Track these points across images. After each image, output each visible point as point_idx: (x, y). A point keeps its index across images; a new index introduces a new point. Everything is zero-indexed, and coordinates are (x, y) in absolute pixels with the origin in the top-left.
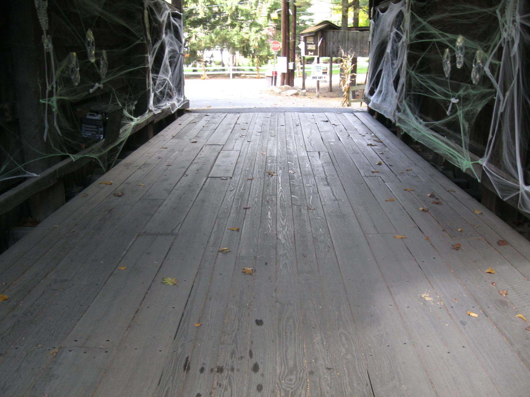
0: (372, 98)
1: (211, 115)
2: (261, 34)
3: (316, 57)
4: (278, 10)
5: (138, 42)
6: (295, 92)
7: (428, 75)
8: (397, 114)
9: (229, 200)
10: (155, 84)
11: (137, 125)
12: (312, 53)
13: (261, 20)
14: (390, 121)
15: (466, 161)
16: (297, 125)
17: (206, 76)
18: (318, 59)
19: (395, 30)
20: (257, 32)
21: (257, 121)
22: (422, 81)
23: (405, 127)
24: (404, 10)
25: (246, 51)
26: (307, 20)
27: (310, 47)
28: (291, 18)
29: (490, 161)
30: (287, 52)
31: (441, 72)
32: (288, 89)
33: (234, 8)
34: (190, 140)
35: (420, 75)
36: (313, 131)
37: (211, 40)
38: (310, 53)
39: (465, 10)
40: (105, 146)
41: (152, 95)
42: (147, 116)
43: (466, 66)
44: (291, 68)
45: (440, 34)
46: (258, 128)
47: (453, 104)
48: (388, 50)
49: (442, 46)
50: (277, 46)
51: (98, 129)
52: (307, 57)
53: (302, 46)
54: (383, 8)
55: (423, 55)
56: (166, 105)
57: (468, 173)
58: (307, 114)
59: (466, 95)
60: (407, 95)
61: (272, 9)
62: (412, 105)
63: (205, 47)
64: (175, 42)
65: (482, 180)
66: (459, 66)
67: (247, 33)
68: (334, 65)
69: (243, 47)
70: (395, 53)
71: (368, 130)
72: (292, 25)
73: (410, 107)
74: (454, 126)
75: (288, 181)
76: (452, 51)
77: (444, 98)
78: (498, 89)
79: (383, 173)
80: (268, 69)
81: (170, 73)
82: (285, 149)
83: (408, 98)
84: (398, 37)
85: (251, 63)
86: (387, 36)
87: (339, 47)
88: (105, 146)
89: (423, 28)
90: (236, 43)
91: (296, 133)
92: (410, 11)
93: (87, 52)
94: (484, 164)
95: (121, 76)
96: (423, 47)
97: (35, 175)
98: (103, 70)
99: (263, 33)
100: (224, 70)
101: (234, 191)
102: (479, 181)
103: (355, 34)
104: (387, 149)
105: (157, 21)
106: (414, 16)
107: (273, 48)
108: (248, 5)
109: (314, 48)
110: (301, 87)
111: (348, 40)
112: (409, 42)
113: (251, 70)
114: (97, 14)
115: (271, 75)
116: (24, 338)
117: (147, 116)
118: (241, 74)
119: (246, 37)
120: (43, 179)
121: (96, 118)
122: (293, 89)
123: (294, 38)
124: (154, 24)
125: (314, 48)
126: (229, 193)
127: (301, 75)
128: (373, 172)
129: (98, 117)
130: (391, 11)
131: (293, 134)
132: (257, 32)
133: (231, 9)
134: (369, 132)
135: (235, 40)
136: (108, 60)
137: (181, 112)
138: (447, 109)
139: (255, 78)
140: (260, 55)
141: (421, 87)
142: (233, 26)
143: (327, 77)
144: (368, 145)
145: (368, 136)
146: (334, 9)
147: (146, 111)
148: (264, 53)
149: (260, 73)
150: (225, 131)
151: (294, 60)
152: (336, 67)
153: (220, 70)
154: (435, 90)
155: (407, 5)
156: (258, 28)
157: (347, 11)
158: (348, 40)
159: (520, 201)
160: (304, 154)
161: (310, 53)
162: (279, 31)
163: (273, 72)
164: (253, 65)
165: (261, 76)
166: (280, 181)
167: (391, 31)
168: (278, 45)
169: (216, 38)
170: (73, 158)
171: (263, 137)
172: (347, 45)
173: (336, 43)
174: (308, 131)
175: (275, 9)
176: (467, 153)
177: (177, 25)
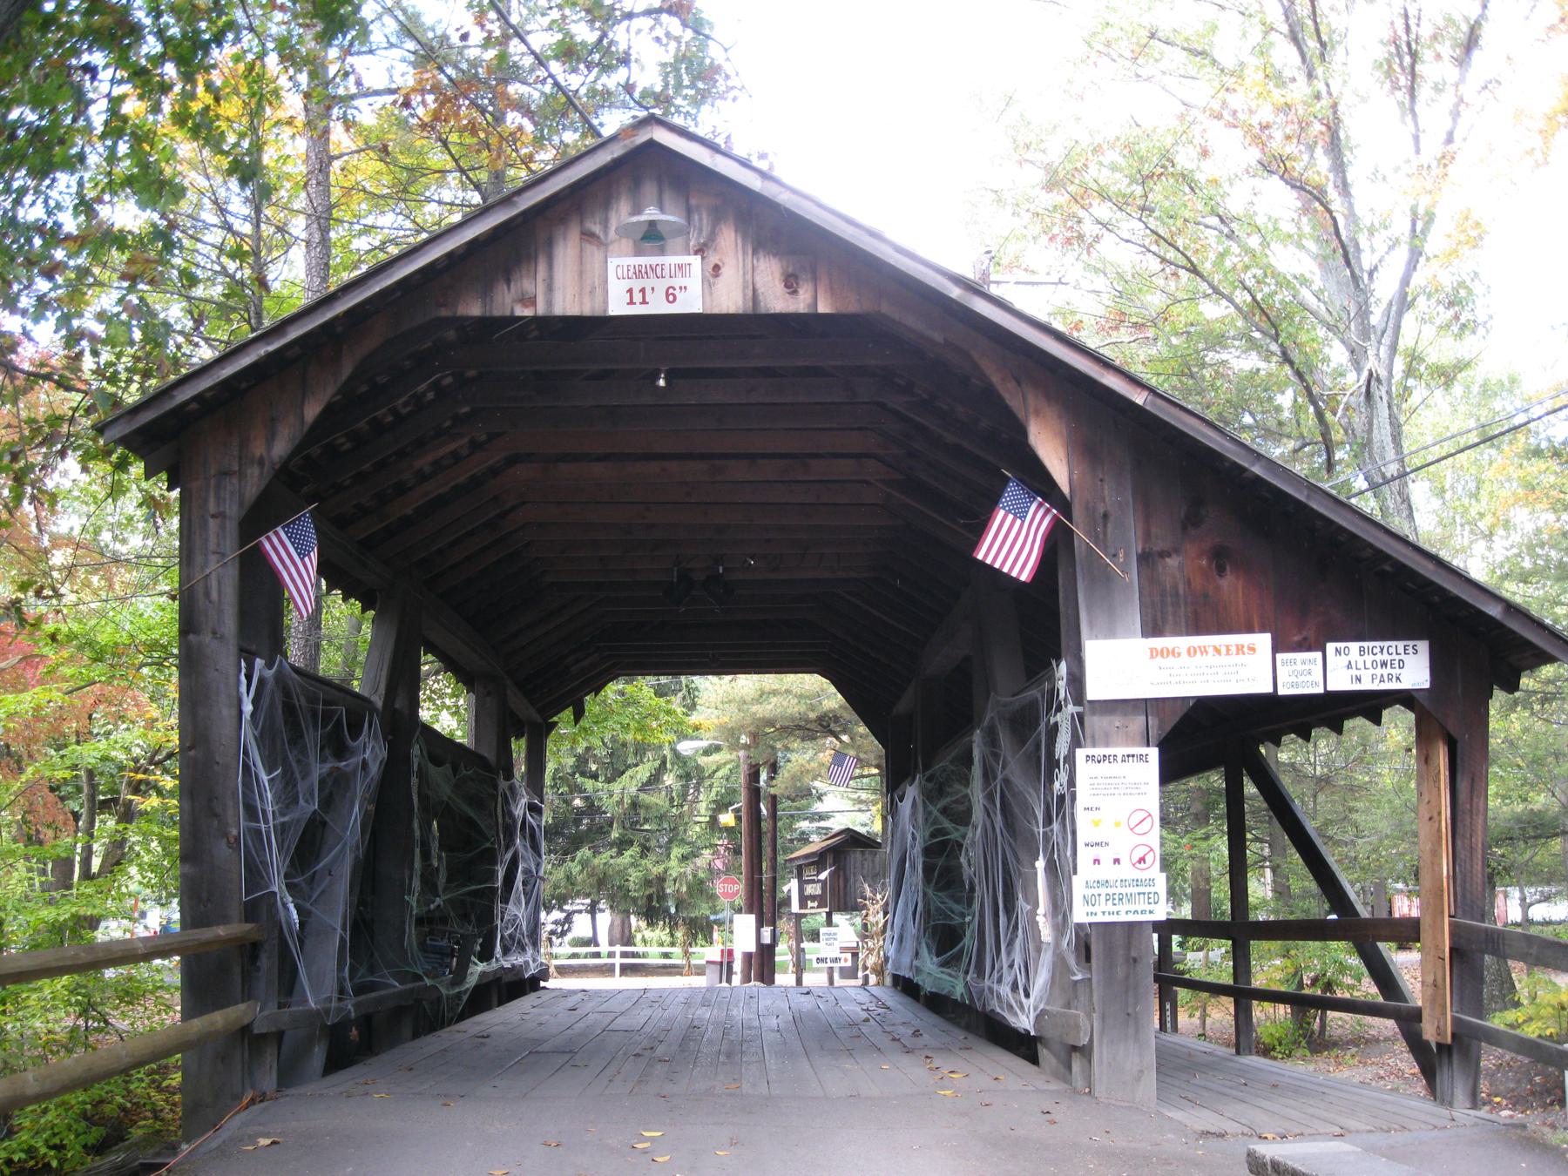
4: (736, 806)
5: (488, 845)
12: (816, 904)
20: (684, 858)
28: (765, 826)
30: (756, 903)
33: (627, 801)
38: (810, 904)
53: (791, 887)
56: (516, 959)
61: (721, 805)
64: (530, 854)
69: (650, 898)
98: (442, 879)
99: (700, 862)
109: (819, 892)
114: (446, 799)
115: (719, 959)
125: (819, 892)
133: (621, 802)
134: (875, 1000)
140: (693, 915)
142: (622, 845)
161: (810, 904)
168: (736, 887)
169: (582, 871)
170: (428, 982)
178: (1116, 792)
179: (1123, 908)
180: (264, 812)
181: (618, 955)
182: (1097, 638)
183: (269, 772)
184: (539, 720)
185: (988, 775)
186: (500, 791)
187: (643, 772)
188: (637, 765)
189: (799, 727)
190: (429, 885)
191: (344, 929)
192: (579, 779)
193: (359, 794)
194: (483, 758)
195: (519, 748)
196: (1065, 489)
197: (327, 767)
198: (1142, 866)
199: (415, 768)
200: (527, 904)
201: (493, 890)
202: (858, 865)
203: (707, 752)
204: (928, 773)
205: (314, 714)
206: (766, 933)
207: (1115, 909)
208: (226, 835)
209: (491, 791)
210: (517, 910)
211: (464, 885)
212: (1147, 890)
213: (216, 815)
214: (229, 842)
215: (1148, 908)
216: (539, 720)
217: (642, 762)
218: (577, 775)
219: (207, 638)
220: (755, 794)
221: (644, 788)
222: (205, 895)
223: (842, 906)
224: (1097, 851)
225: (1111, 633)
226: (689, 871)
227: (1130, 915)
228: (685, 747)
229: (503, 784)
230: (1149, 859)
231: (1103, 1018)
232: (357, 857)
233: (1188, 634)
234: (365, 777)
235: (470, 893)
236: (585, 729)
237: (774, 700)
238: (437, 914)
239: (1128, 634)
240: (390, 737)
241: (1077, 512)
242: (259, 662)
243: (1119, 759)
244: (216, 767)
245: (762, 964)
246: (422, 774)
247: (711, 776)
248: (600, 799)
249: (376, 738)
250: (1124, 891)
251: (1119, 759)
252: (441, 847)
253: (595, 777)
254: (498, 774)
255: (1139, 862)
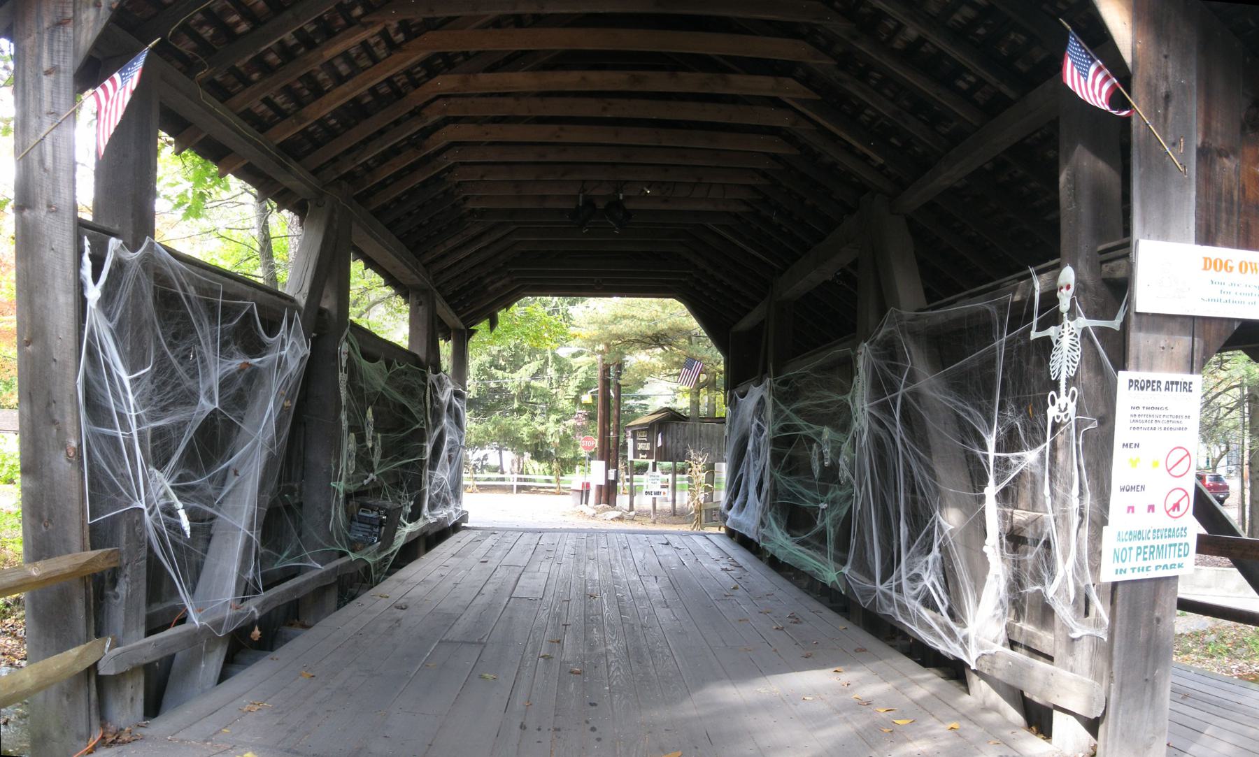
0: (729, 513)
1: (501, 533)
2: (564, 425)
3: (650, 462)
4: (593, 390)
5: (418, 426)
6: (617, 514)
7: (797, 478)
8: (761, 530)
9: (543, 617)
10: (430, 483)
11: (411, 534)
12: (645, 456)
13: (564, 404)
14: (752, 540)
15: (831, 573)
16: (625, 548)
17: (475, 487)
18: (654, 465)
19: (756, 421)
20: (558, 421)
21: (568, 542)
22: (789, 485)
23: (770, 546)
24: (766, 395)
25: (539, 451)
26: (637, 407)
27: (641, 446)
28: (613, 404)
29: (854, 567)
31: (810, 471)
32: (608, 510)
33: (523, 385)
34: (478, 559)
35: (787, 478)
36: (647, 555)
37: (487, 432)
39: (826, 397)
40: (380, 551)
41: (427, 497)
42: (421, 523)
43: (834, 464)
44: (612, 477)
45: (806, 425)
46: (569, 549)
47: (823, 510)
48: (750, 448)
49: (810, 441)
50: (590, 443)
51: (372, 529)
52: (638, 462)
54: (742, 391)
55: (789, 452)
56: (442, 513)
57: (834, 586)
58: (638, 536)
59: (834, 498)
60: (772, 505)
61: (583, 389)
62: (779, 516)
63: (476, 444)
64: (454, 429)
65: (846, 591)
66: (826, 463)
67: (542, 424)
68: (678, 476)
70: (757, 451)
71: (722, 553)
72: (614, 413)
73: (776, 519)
74: (822, 536)
75: (616, 603)
76: (820, 446)
77: (813, 505)
78: (855, 485)
79: (739, 597)
80: (575, 479)
81: (449, 470)
82: (610, 573)
83: (773, 509)
84: (760, 430)
85: (547, 471)
86: (747, 430)
87: (687, 447)
88: (380, 551)
89: (787, 418)
90: (526, 438)
91: (625, 556)
92: (771, 397)
93: (365, 433)
94: (846, 572)
95: (394, 468)
96: (789, 441)
97: (319, 566)
98: (376, 459)
100: (503, 479)
101: (548, 611)
102: (843, 592)
103: (710, 428)
104: (747, 574)
105: (438, 400)
106: (962, 417)
107: (583, 447)
108: (546, 381)
109: (648, 448)
110: (628, 508)
111: (700, 436)
112: (771, 436)
113: (548, 481)
114: (380, 389)
115: (581, 489)
116: (981, 31)
117: (421, 523)
118: (531, 487)
119: (541, 428)
120: (327, 572)
121: (371, 515)
122: (615, 510)
123: (618, 432)
124: (436, 406)
125: (648, 448)
126: (541, 612)
127: (627, 491)
128: (726, 596)
129: (374, 515)
130: (752, 396)
131: (619, 558)
132: (558, 421)
134: (725, 556)
135: (525, 433)
136: (382, 446)
137: (456, 528)
138: (817, 518)
139: (554, 493)
141: (790, 494)
142: (520, 411)
143: (669, 492)
144: (723, 569)
145: (724, 561)
146: (679, 391)
147: (419, 518)
148: (568, 455)
149: (561, 485)
150: (524, 552)
151: (616, 466)
152: (682, 479)
153: (498, 479)
154: (803, 496)
155: (768, 389)
156: (559, 416)
157: (698, 394)
158: (700, 436)
159: (877, 604)
160: (635, 578)
162: (593, 423)
163: (583, 484)
164: (551, 474)
165: (563, 491)
166: (606, 603)
167: (752, 423)
169: (494, 429)
170: (353, 556)
171: (579, 560)
172: (698, 443)
173: (681, 441)
174: (641, 555)
175: (588, 389)
176: (832, 564)
177: (459, 406)
178: (1157, 425)
179: (1152, 563)
180: (122, 417)
181: (516, 480)
182: (1149, 237)
183: (132, 371)
184: (463, 327)
185: (881, 386)
186: (429, 382)
187: (533, 367)
188: (529, 363)
189: (638, 341)
190: (363, 460)
191: (251, 529)
192: (494, 371)
193: (274, 390)
194: (415, 356)
195: (446, 348)
196: (1128, 58)
197: (236, 363)
198: (1176, 513)
199: (344, 364)
200: (451, 469)
201: (422, 463)
202: (675, 432)
203: (574, 356)
204: (781, 378)
205: (211, 307)
206: (612, 472)
207: (1145, 564)
208: (64, 446)
209: (422, 383)
210: (443, 474)
211: (397, 459)
212: (1177, 540)
213: (54, 422)
214: (68, 455)
215: (1177, 561)
216: (463, 327)
217: (533, 360)
218: (493, 368)
219: (42, 212)
220: (606, 383)
221: (534, 377)
222: (45, 514)
223: (663, 458)
224: (1132, 497)
225: (1164, 235)
226: (561, 430)
227: (1160, 570)
228: (563, 352)
229: (431, 377)
230: (1183, 505)
231: (1121, 688)
232: (270, 455)
233: (1238, 247)
234: (282, 373)
235: (401, 466)
236: (499, 336)
237: (624, 322)
238: (371, 487)
239: (1183, 239)
240: (314, 335)
241: (1138, 85)
242: (114, 243)
243: (1163, 386)
244: (53, 365)
245: (608, 493)
246: (352, 369)
247: (576, 371)
248: (506, 383)
249: (297, 335)
250: (1155, 542)
251: (1163, 386)
252: (376, 429)
253: (504, 369)
254: (427, 369)
255: (1173, 509)
